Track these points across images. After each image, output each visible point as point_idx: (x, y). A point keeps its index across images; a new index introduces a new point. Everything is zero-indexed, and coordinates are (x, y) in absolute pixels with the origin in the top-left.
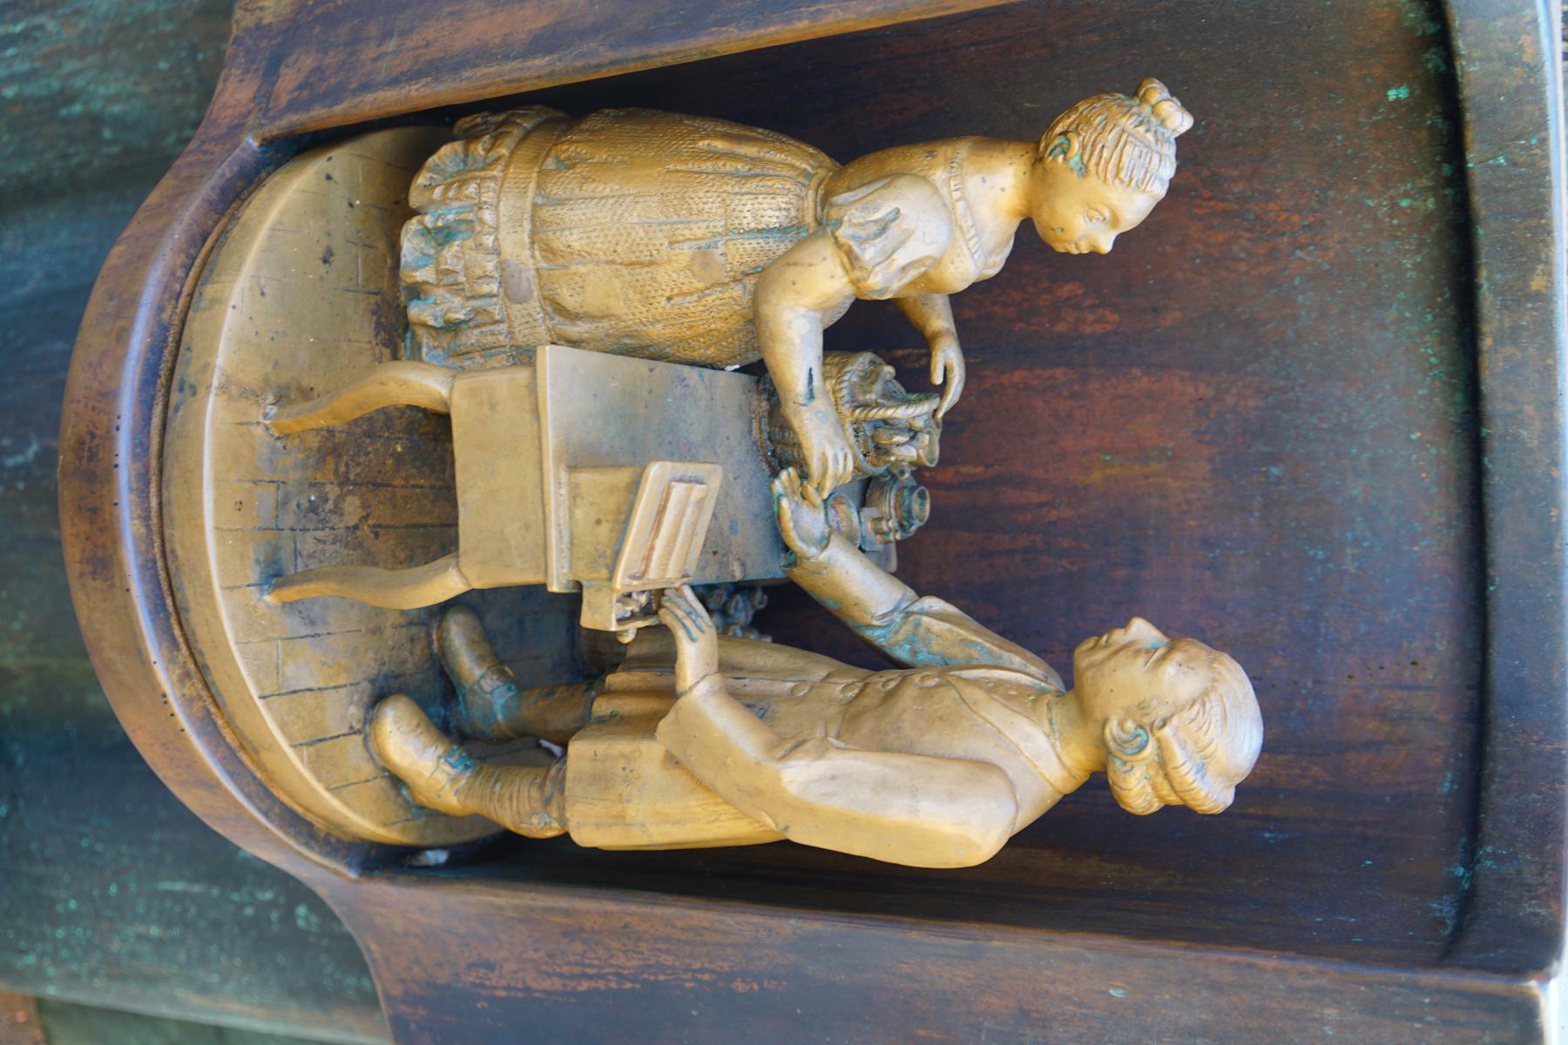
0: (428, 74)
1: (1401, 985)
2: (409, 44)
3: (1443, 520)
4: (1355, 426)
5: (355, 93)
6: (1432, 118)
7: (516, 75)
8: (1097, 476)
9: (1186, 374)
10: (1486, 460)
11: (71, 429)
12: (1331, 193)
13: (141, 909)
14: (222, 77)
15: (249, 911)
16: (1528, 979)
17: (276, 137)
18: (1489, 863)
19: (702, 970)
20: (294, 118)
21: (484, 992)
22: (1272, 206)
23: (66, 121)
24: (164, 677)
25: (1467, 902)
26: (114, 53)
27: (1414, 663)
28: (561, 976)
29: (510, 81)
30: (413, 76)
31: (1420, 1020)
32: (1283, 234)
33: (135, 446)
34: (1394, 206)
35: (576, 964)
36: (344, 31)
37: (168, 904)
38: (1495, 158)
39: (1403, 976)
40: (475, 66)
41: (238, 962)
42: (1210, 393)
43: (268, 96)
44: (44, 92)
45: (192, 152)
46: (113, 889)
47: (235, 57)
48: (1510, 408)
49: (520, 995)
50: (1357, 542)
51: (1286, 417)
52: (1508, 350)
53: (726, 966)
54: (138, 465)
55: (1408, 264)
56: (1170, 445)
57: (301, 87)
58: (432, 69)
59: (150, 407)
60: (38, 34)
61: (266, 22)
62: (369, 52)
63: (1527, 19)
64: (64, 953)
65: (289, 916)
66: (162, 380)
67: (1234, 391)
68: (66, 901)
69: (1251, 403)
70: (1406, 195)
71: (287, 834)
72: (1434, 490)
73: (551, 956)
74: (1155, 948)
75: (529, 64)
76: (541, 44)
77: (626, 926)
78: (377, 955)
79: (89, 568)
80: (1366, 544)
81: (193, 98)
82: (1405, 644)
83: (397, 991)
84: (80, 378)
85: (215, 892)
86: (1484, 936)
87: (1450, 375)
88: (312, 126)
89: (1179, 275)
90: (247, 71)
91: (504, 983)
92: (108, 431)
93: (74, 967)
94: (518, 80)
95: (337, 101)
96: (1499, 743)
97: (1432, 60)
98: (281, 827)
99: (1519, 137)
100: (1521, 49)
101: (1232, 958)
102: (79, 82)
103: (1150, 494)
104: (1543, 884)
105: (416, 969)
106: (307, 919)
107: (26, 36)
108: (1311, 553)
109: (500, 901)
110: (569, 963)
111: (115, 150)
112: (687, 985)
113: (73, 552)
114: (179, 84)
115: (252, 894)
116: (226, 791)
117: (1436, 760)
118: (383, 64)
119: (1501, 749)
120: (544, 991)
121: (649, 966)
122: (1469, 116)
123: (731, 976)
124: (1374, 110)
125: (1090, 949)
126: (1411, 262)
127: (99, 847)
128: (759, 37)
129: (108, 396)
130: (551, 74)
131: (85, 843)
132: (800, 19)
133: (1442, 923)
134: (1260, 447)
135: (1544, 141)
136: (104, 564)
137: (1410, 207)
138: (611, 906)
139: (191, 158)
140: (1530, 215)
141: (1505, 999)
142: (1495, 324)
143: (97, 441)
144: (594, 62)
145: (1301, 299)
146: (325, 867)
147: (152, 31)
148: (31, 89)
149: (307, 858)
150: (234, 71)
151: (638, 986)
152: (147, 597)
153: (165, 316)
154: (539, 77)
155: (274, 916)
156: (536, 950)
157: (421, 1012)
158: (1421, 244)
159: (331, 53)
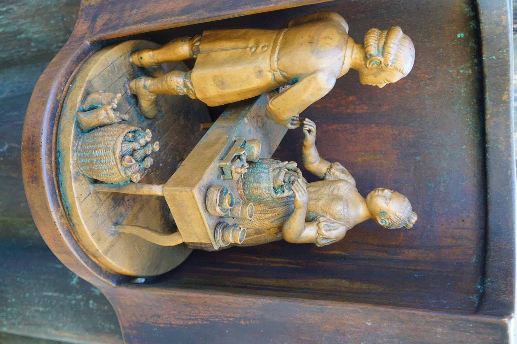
0: (147, 21)
1: (462, 320)
2: (140, 11)
3: (473, 174)
4: (444, 144)
5: (122, 27)
6: (472, 44)
7: (176, 21)
8: (360, 160)
9: (389, 126)
10: (487, 155)
11: (26, 135)
12: (438, 68)
13: (37, 301)
14: (77, 22)
15: (73, 302)
16: (504, 318)
17: (95, 41)
18: (489, 284)
19: (230, 317)
20: (102, 35)
21: (156, 325)
22: (419, 72)
23: (19, 40)
24: (55, 216)
25: (482, 296)
26: (36, 18)
27: (463, 221)
28: (182, 319)
29: (174, 23)
30: (142, 21)
31: (469, 332)
32: (422, 81)
33: (47, 140)
34: (458, 72)
35: (188, 315)
36: (118, 7)
37: (46, 300)
38: (492, 56)
39: (464, 317)
40: (163, 18)
41: (69, 319)
42: (397, 133)
43: (93, 28)
44: (12, 30)
45: (67, 45)
46: (27, 295)
47: (82, 15)
48: (495, 138)
49: (168, 326)
50: (445, 182)
51: (422, 141)
52: (495, 119)
53: (238, 316)
54: (48, 146)
55: (462, 91)
56: (384, 149)
57: (104, 25)
58: (148, 19)
59: (53, 127)
60: (11, 11)
61: (92, 4)
62: (127, 14)
63: (504, 11)
64: (10, 316)
65: (87, 304)
66: (57, 119)
67: (405, 132)
68: (11, 299)
69: (411, 136)
70: (462, 69)
71: (93, 270)
72: (470, 165)
73: (179, 312)
74: (382, 309)
75: (180, 18)
76: (184, 11)
77: (205, 302)
78: (120, 313)
79: (31, 180)
80: (448, 182)
81: (62, 33)
82: (460, 215)
83: (127, 325)
84: (29, 118)
85: (62, 296)
86: (488, 303)
87: (476, 128)
88: (108, 38)
89: (388, 94)
90: (85, 20)
91: (163, 322)
92: (39, 134)
93: (13, 321)
94: (177, 23)
95: (116, 29)
96: (492, 245)
97: (472, 24)
98: (91, 268)
99: (500, 50)
100: (502, 20)
101: (407, 311)
102: (24, 27)
103: (377, 165)
104: (507, 290)
105: (133, 318)
106: (93, 305)
107: (7, 12)
108: (430, 185)
109: (163, 294)
110: (185, 315)
111: (35, 50)
112: (225, 322)
113: (26, 174)
114: (58, 28)
115: (74, 296)
116: (74, 255)
117: (471, 252)
118: (132, 17)
119: (492, 248)
120: (176, 325)
121: (213, 316)
122: (484, 43)
123: (240, 319)
124: (453, 41)
125: (361, 309)
126: (464, 91)
127: (23, 281)
128: (258, 9)
129: (39, 123)
130: (188, 21)
131: (18, 279)
132: (271, 4)
133: (474, 302)
134: (413, 150)
135: (508, 51)
136: (36, 178)
137: (463, 73)
138: (201, 295)
139: (67, 47)
140: (503, 75)
141: (497, 324)
142: (491, 111)
143: (35, 138)
144: (202, 17)
145: (427, 102)
146: (104, 282)
147: (49, 11)
148: (8, 29)
149: (99, 279)
150: (81, 20)
151: (208, 322)
152: (50, 190)
153: (58, 98)
154: (184, 22)
155: (82, 304)
156: (175, 311)
157: (135, 332)
158: (467, 85)
159: (114, 14)
